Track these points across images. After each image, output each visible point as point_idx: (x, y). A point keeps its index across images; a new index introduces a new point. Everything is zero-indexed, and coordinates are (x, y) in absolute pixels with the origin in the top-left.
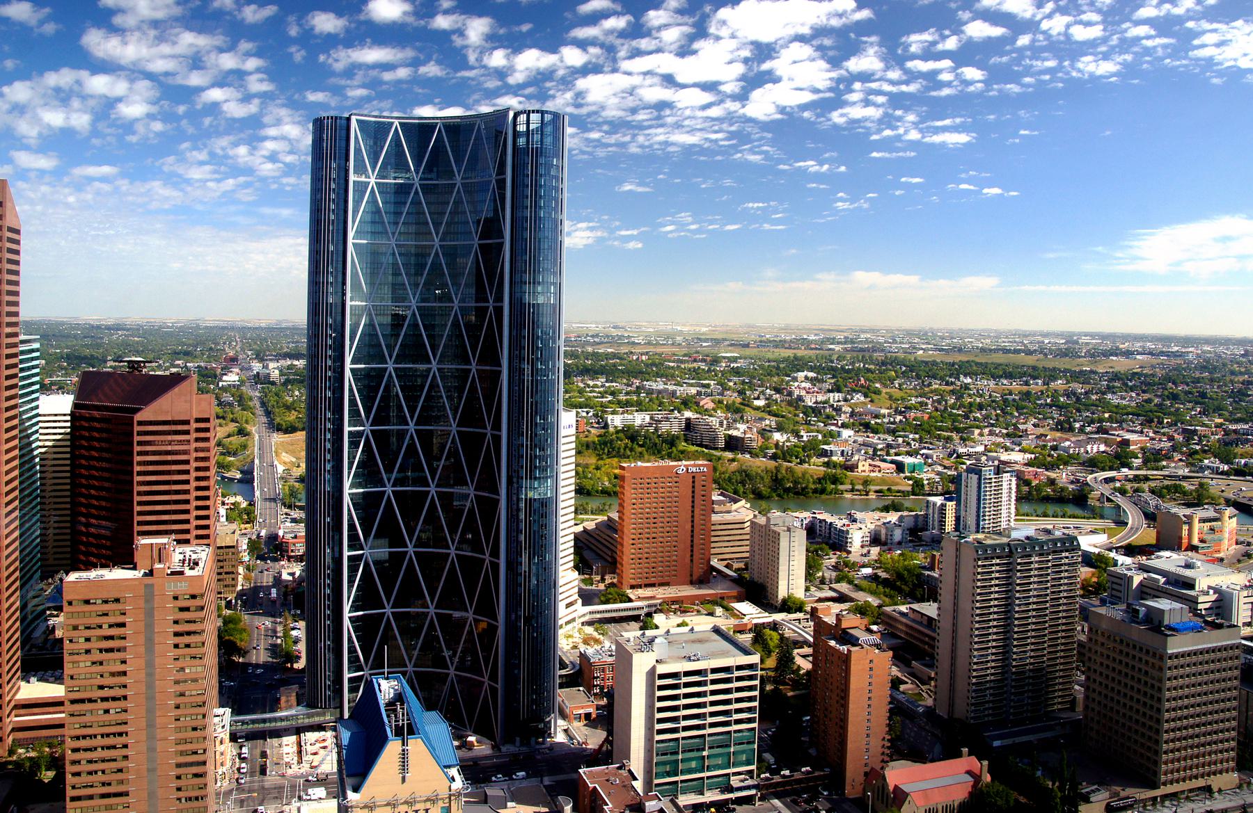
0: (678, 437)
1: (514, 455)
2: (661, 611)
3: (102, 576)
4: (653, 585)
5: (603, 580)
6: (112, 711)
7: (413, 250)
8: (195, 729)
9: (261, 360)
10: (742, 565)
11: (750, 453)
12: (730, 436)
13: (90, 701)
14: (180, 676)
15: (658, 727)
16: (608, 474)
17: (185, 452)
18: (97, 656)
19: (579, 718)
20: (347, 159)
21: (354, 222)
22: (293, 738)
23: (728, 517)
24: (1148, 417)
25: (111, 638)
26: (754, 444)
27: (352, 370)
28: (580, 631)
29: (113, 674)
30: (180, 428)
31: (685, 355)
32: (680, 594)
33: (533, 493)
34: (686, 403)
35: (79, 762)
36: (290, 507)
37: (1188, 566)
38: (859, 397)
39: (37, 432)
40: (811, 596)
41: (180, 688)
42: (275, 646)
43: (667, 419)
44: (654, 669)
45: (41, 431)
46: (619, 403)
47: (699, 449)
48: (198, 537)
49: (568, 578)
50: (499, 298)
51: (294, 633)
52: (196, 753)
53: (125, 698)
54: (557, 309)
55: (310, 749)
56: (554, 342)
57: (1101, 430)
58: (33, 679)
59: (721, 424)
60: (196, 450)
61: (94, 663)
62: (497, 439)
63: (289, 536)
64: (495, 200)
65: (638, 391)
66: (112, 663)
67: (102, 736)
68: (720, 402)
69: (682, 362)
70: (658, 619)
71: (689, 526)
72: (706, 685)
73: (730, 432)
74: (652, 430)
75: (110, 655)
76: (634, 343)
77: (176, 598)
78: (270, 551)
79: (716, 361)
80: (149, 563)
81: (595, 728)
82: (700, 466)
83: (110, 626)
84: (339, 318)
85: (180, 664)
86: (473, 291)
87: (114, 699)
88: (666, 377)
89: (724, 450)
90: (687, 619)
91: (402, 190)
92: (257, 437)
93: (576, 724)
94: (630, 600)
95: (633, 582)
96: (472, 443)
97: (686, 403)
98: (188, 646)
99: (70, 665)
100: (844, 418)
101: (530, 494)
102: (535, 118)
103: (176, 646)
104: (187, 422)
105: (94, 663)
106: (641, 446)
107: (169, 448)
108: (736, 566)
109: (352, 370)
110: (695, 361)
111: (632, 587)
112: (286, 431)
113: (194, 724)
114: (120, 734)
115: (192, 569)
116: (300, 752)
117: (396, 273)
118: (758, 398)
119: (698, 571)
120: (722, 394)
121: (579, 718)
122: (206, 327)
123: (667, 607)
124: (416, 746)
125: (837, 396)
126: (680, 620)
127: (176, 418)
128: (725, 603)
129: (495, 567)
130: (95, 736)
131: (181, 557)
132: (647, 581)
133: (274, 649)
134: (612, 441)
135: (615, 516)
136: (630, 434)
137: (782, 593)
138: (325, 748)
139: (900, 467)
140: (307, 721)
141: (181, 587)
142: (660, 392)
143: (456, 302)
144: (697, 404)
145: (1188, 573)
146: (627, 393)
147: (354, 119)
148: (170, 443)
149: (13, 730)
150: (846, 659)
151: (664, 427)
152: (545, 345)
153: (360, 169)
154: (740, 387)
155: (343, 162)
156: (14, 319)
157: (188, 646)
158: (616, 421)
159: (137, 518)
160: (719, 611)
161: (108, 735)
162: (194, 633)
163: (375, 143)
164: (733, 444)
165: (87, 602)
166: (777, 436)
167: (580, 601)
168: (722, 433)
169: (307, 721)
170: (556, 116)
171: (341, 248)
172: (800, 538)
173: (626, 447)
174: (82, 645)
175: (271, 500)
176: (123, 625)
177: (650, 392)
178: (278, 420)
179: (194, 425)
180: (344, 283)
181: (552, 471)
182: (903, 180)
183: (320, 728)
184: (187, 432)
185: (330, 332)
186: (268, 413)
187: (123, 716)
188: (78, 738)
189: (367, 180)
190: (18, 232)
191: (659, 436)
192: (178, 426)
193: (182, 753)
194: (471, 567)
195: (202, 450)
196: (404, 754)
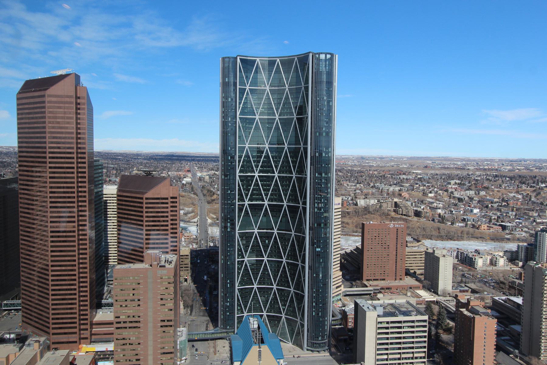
2: (380, 292)
4: (377, 280)
21: (238, 222)
30: (164, 201)
59: (412, 204)
70: (379, 296)
71: (395, 253)
94: (367, 287)
96: (293, 210)
97: (394, 194)
104: (167, 199)
111: (367, 280)
118: (431, 192)
124: (265, 348)
139: (504, 228)
158: (362, 203)
167: (342, 286)
194: (293, 267)
196: (260, 352)
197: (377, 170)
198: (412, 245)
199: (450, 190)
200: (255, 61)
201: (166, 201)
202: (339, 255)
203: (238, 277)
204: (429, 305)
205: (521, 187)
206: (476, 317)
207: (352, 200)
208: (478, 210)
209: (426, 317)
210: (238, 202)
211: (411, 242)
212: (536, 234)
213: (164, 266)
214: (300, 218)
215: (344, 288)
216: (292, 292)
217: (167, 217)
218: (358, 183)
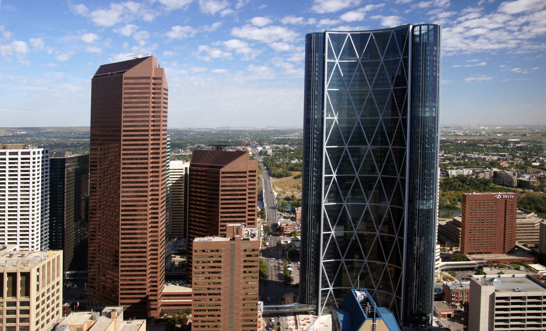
0: (489, 181)
1: (413, 189)
2: (487, 266)
3: (210, 240)
5: (451, 250)
6: (213, 300)
7: (358, 93)
8: (252, 310)
9: (261, 145)
10: (533, 245)
11: (533, 189)
12: (521, 181)
13: (204, 294)
14: (246, 286)
15: (496, 324)
16: (449, 199)
17: (245, 186)
18: (207, 275)
19: (444, 316)
20: (324, 52)
21: (328, 81)
22: (293, 317)
23: (524, 221)
25: (215, 267)
26: (535, 185)
27: (327, 149)
28: (441, 274)
29: (214, 283)
30: (242, 175)
31: (488, 141)
32: (497, 258)
33: (423, 206)
34: (493, 164)
35: (197, 321)
36: (282, 211)
39: (168, 177)
41: (246, 291)
42: (280, 274)
43: (483, 172)
44: (493, 294)
45: (170, 176)
46: (454, 164)
47: (502, 187)
48: (249, 224)
50: (405, 114)
51: (289, 269)
52: (252, 321)
53: (220, 294)
54: (435, 120)
55: (302, 323)
56: (435, 134)
58: (169, 284)
59: (514, 174)
60: (249, 185)
61: (205, 278)
62: (403, 181)
63: (283, 225)
64: (402, 68)
65: (464, 158)
66: (214, 278)
67: (209, 310)
68: (512, 163)
69: (487, 144)
70: (486, 270)
71: (503, 225)
72: (541, 304)
73: (521, 178)
74: (474, 177)
75: (213, 275)
76: (457, 135)
77: (245, 251)
78: (274, 231)
79: (507, 143)
80: (232, 234)
81: (454, 321)
82: (509, 195)
83: (214, 262)
84: (320, 125)
85: (246, 280)
86: (390, 110)
87: (214, 294)
88: (479, 151)
89: (517, 187)
90: (503, 271)
91: (352, 66)
92: (263, 180)
93: (442, 319)
94: (469, 260)
95: (470, 251)
96: (389, 183)
97: (493, 164)
98: (250, 272)
99: (195, 278)
101: (421, 207)
102: (424, 28)
103: (245, 272)
104: (245, 172)
105: (205, 278)
106: (468, 185)
107: (236, 184)
108: (529, 245)
109: (327, 149)
110: (494, 143)
111: (470, 254)
112: (278, 177)
113: (252, 307)
114: (217, 310)
115: (252, 237)
116: (296, 324)
117: (349, 103)
118: (535, 162)
119: (508, 249)
120: (513, 159)
121: (444, 316)
122: (232, 131)
123: (490, 264)
124: (379, 323)
126: (499, 271)
127: (240, 171)
128: (525, 264)
129: (401, 241)
130: (205, 310)
131: (247, 232)
132: (477, 251)
133: (279, 275)
134: (451, 183)
135: (459, 219)
136: (462, 179)
138: (309, 322)
140: (299, 309)
141: (248, 246)
142: (476, 159)
143: (400, 116)
144: (499, 164)
146: (457, 159)
147: (327, 33)
148: (237, 182)
149: (162, 305)
151: (481, 176)
152: (430, 136)
153: (331, 56)
154: (524, 156)
155: (322, 54)
156: (165, 128)
157: (250, 272)
158: (453, 173)
159: (220, 215)
160: (522, 268)
161: (211, 310)
162: (253, 266)
163: (338, 44)
164: (522, 184)
165: (204, 251)
167: (440, 259)
168: (515, 179)
169: (299, 309)
170: (436, 26)
171: (321, 93)
173: (459, 185)
174: (201, 270)
175: (272, 208)
176: (220, 262)
177: (470, 158)
178: (273, 172)
179: (248, 174)
180: (323, 109)
181: (433, 196)
183: (306, 313)
184: (245, 177)
185: (315, 131)
186: (268, 169)
187: (218, 302)
188: (197, 311)
189: (334, 61)
190: (167, 90)
191: (478, 180)
192: (240, 174)
193: (245, 321)
195: (252, 185)
196: (373, 327)
197: (466, 140)
200: (347, 34)
201: (244, 175)
210: (325, 174)
211: (519, 214)
215: (442, 261)
218: (445, 153)
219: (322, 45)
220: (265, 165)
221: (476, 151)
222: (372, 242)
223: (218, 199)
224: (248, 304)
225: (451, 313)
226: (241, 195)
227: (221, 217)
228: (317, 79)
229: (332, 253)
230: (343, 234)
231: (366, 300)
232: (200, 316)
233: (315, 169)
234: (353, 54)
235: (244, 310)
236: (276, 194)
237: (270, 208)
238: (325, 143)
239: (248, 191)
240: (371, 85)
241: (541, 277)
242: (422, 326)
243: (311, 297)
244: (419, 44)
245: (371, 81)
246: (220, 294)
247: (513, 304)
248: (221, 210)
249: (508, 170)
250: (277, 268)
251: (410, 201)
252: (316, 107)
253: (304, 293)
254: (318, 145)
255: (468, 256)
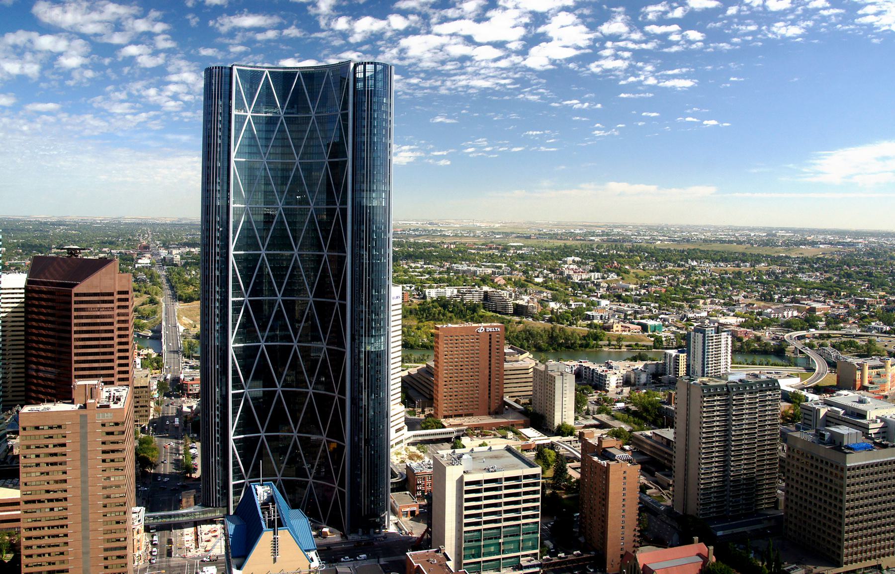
0: (478, 306)
2: (467, 435)
3: (48, 409)
4: (460, 416)
5: (423, 412)
6: (56, 509)
7: (279, 166)
8: (118, 523)
9: (167, 248)
10: (527, 401)
11: (532, 317)
12: (517, 305)
13: (40, 501)
14: (107, 483)
16: (426, 333)
17: (110, 317)
18: (44, 468)
19: (406, 514)
20: (230, 99)
21: (235, 145)
22: (192, 529)
23: (516, 365)
24: (830, 291)
25: (55, 455)
26: (535, 311)
28: (406, 449)
29: (56, 482)
30: (106, 298)
31: (483, 245)
33: (371, 346)
34: (484, 280)
35: (31, 547)
36: (189, 357)
37: (861, 401)
38: (613, 276)
40: (579, 423)
42: (177, 460)
43: (470, 292)
44: (462, 478)
49: (397, 410)
50: (344, 202)
51: (192, 451)
53: (66, 499)
54: (387, 210)
57: (794, 301)
59: (510, 296)
61: (42, 473)
62: (343, 307)
63: (188, 379)
64: (340, 129)
65: (448, 271)
66: (56, 473)
67: (49, 528)
68: (510, 279)
69: (481, 249)
70: (465, 440)
72: (501, 490)
73: (517, 302)
74: (459, 300)
75: (55, 467)
76: (444, 235)
77: (103, 425)
78: (174, 390)
79: (506, 249)
81: (419, 521)
83: (55, 446)
84: (225, 217)
85: (106, 474)
86: (324, 196)
87: (57, 500)
88: (469, 261)
89: (513, 315)
90: (487, 441)
91: (271, 122)
92: (164, 305)
93: (404, 519)
94: (444, 427)
95: (446, 413)
96: (324, 309)
97: (484, 280)
98: (112, 461)
99: (25, 475)
100: (602, 291)
101: (368, 348)
103: (104, 461)
104: (112, 294)
105: (42, 473)
106: (451, 312)
108: (523, 401)
110: (490, 249)
111: (445, 417)
112: (186, 301)
113: (118, 519)
114: (62, 526)
116: (197, 540)
117: (267, 184)
118: (538, 277)
119: (494, 405)
120: (511, 273)
121: (406, 514)
123: (471, 432)
124: (283, 535)
125: (597, 275)
126: (481, 442)
128: (515, 429)
130: (43, 528)
131: (108, 394)
132: (456, 413)
133: (177, 463)
134: (429, 308)
135: (432, 364)
136: (443, 303)
137: (557, 421)
138: (215, 536)
139: (644, 328)
140: (202, 516)
141: (107, 417)
142: (464, 272)
144: (492, 281)
145: (861, 407)
146: (440, 273)
147: (235, 68)
150: (606, 470)
151: (468, 298)
152: (379, 237)
153: (241, 106)
155: (227, 100)
157: (112, 461)
158: (432, 293)
159: (74, 366)
160: (510, 435)
161: (53, 527)
162: (117, 451)
163: (251, 87)
164: (520, 311)
165: (37, 428)
166: (552, 305)
167: (406, 427)
168: (511, 302)
171: (226, 165)
172: (571, 381)
175: (174, 352)
176: (64, 445)
177: (457, 272)
178: (179, 292)
179: (117, 296)
180: (228, 191)
182: (644, 114)
183: (212, 521)
184: (112, 302)
185: (218, 227)
186: (172, 288)
187: (64, 513)
188: (30, 529)
189: (245, 114)
191: (464, 305)
192: (105, 297)
193: (108, 541)
194: (324, 402)
195: (123, 315)
196: (275, 541)
197: (455, 243)
198: (512, 358)
199: (566, 272)
202: (400, 379)
203: (234, 328)
204: (540, 450)
205: (666, 266)
206: (611, 463)
207: (417, 289)
208: (608, 302)
209: (538, 470)
212: (689, 334)
213: (108, 406)
214: (336, 320)
216: (325, 440)
217: (112, 331)
219: (227, 87)
220: (168, 281)
221: (465, 261)
222: (304, 404)
223: (70, 339)
224: (111, 513)
225: (415, 508)
226: (106, 331)
227: (76, 369)
228: (219, 141)
229: (247, 424)
230: (261, 394)
231: (271, 499)
232: (36, 538)
233: (217, 289)
234: (270, 103)
235: (106, 523)
236: (182, 329)
237: (171, 351)
238: (232, 247)
239: (117, 326)
240: (297, 154)
241: (533, 447)
242: (375, 533)
243: (218, 496)
244: (363, 92)
245: (297, 147)
246: (66, 499)
247: (487, 490)
248: (75, 358)
249: (503, 290)
250: (174, 451)
251: (353, 339)
252: (218, 188)
253: (208, 490)
254: (221, 249)
255: (443, 420)
